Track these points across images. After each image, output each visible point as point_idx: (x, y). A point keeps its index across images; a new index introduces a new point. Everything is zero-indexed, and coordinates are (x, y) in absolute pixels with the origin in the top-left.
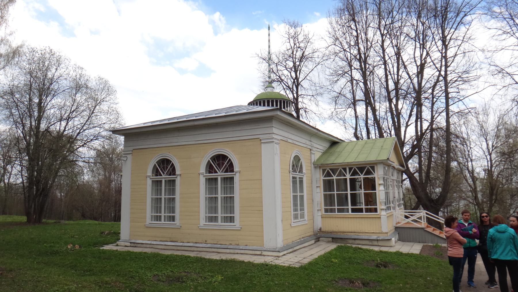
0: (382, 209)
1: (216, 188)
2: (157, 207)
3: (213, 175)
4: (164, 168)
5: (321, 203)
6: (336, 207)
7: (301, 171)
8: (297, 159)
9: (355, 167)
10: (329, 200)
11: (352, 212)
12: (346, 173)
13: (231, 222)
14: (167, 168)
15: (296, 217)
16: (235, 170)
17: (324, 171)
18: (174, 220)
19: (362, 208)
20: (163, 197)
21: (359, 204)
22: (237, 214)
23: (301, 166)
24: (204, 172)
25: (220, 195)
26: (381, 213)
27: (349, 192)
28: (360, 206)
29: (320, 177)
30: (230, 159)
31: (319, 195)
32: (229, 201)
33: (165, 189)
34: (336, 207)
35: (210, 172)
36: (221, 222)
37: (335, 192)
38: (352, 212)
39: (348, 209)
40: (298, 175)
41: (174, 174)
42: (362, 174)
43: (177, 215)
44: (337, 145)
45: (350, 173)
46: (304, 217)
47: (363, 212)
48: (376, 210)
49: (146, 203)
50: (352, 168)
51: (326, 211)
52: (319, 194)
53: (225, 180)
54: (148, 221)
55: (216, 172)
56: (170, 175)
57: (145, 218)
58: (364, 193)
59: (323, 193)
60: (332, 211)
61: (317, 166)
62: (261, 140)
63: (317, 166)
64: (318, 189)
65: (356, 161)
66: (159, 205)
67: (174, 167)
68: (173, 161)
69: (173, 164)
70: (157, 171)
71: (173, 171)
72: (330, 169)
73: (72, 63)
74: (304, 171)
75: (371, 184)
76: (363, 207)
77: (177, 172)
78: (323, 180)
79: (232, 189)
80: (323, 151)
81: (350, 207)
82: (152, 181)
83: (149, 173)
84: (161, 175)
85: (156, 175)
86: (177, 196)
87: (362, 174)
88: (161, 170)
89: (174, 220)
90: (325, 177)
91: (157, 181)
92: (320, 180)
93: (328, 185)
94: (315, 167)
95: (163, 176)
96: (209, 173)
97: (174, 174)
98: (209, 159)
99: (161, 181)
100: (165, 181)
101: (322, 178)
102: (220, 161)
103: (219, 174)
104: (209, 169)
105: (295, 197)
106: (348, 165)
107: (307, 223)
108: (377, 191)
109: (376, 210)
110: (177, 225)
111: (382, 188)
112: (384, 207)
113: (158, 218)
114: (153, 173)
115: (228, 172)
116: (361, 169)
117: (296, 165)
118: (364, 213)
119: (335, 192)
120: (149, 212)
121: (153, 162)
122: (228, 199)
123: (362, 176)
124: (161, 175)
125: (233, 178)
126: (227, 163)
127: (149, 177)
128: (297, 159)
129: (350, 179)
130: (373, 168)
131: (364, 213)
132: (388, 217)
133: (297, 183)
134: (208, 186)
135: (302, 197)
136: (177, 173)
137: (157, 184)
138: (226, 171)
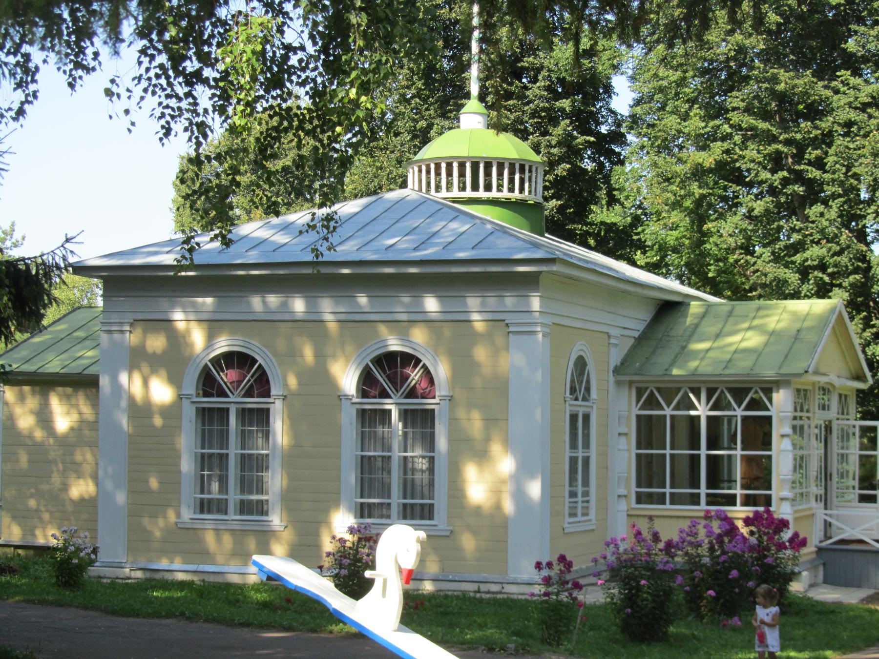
0: (782, 499)
3: (215, 401)
5: (628, 479)
8: (581, 364)
9: (722, 387)
11: (639, 501)
13: (430, 519)
16: (272, 394)
17: (640, 393)
19: (664, 494)
21: (726, 485)
23: (588, 382)
27: (703, 452)
28: (729, 488)
35: (206, 394)
36: (235, 514)
38: (709, 503)
39: (699, 495)
42: (739, 407)
46: (587, 514)
47: (664, 503)
50: (716, 389)
51: (640, 499)
53: (246, 415)
58: (743, 456)
59: (634, 451)
64: (623, 438)
65: (727, 372)
68: (260, 361)
72: (659, 390)
74: (594, 394)
75: (759, 432)
76: (738, 491)
78: (638, 417)
81: (703, 491)
82: (197, 408)
89: (431, 518)
90: (711, 409)
92: (628, 417)
93: (648, 431)
97: (267, 394)
98: (367, 361)
100: (237, 409)
101: (636, 411)
104: (204, 385)
105: (573, 461)
106: (704, 382)
107: (593, 527)
108: (774, 453)
110: (440, 527)
111: (786, 444)
112: (787, 493)
115: (252, 397)
116: (739, 393)
118: (668, 506)
119: (668, 452)
122: (216, 461)
123: (740, 412)
124: (227, 396)
125: (268, 410)
126: (252, 377)
127: (188, 397)
128: (581, 364)
131: (668, 506)
135: (586, 461)
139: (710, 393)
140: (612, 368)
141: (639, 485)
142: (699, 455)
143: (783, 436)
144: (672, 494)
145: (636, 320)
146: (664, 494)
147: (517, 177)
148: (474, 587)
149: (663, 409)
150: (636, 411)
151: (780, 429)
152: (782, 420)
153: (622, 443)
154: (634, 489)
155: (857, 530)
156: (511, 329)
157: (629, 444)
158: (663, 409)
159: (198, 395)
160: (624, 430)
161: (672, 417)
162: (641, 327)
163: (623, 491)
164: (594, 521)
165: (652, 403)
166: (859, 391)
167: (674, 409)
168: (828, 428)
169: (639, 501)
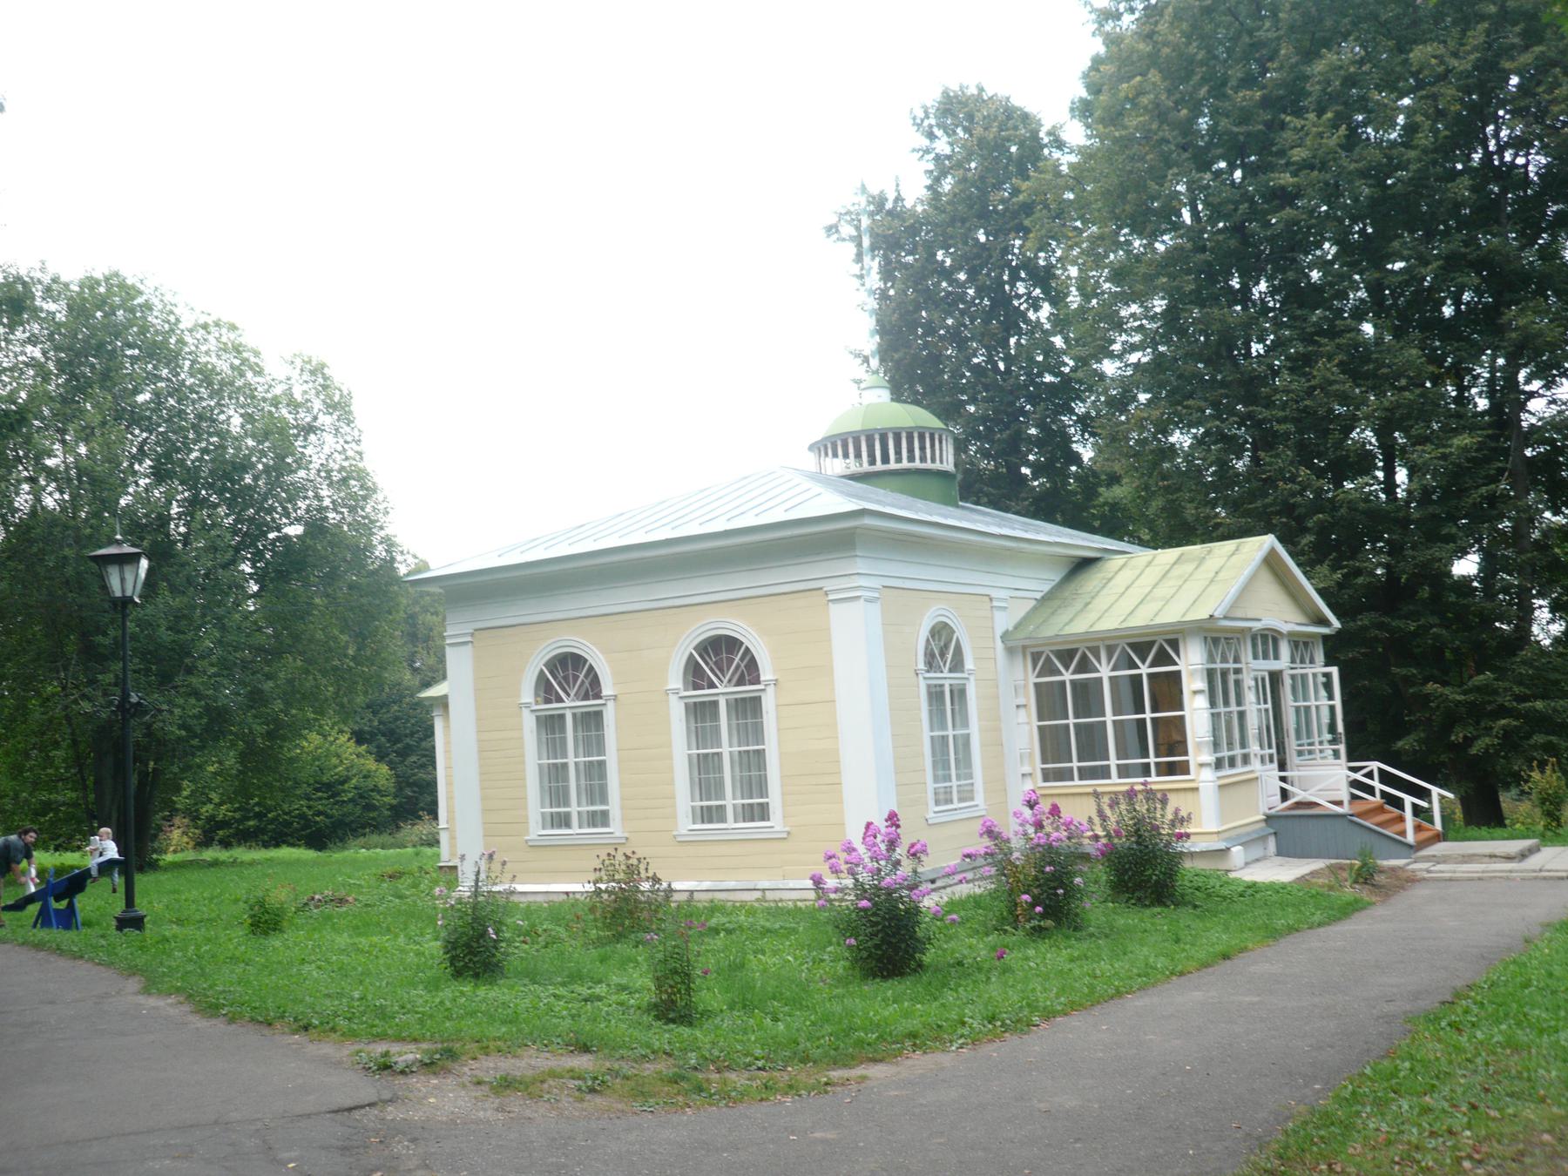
0: (1202, 765)
1: (716, 730)
2: (1239, 703)
4: (566, 678)
5: (1031, 755)
6: (1075, 764)
7: (958, 665)
8: (941, 632)
9: (1160, 640)
10: (1052, 745)
11: (1046, 779)
12: (1099, 662)
13: (763, 819)
14: (576, 678)
15: (943, 798)
17: (1036, 657)
18: (605, 823)
19: (1071, 769)
20: (571, 760)
22: (774, 799)
23: (958, 649)
24: (680, 685)
25: (727, 749)
26: (1198, 774)
29: (1022, 680)
30: (747, 649)
31: (1023, 730)
32: (753, 762)
33: (576, 738)
34: (1075, 764)
35: (696, 687)
37: (1071, 721)
40: (946, 678)
41: (598, 696)
43: (614, 806)
44: (1100, 564)
45: (1109, 660)
48: (1183, 768)
49: (524, 779)
51: (1047, 776)
52: (1027, 728)
54: (536, 831)
55: (712, 685)
56: (586, 698)
57: (525, 822)
59: (1036, 723)
60: (1065, 775)
61: (1018, 646)
62: (826, 594)
63: (1018, 646)
64: (1022, 711)
66: (1234, 708)
67: (596, 676)
68: (590, 661)
69: (591, 668)
70: (548, 688)
71: (593, 687)
73: (388, 531)
74: (969, 664)
75: (1168, 690)
77: (607, 690)
79: (758, 733)
80: (1038, 596)
81: (1113, 762)
82: (538, 718)
83: (527, 695)
84: (561, 701)
85: (548, 701)
86: (611, 757)
87: (1143, 662)
88: (560, 684)
89: (605, 823)
91: (552, 716)
92: (1025, 686)
93: (1049, 701)
94: (1010, 651)
95: (568, 703)
96: (695, 689)
97: (598, 696)
99: (562, 717)
100: (574, 715)
101: (1033, 679)
102: (721, 654)
103: (721, 689)
105: (940, 745)
106: (1102, 639)
108: (1187, 713)
109: (1183, 768)
110: (617, 834)
111: (1202, 702)
113: (563, 821)
114: (537, 695)
117: (942, 648)
119: (1071, 721)
120: (535, 807)
121: (536, 663)
124: (561, 701)
126: (742, 659)
127: (527, 705)
128: (941, 632)
129: (1111, 678)
130: (1174, 644)
131: (1077, 782)
132: (1221, 787)
133: (946, 703)
134: (693, 725)
136: (604, 693)
137: (551, 725)
138: (740, 682)
139: (1110, 650)
140: (999, 633)
141: (1044, 761)
142: (1104, 723)
143: (1195, 692)
144: (1080, 769)
145: (1039, 583)
146: (1071, 769)
147: (928, 451)
148: (758, 895)
149: (1060, 674)
150: (1033, 679)
151: (1193, 684)
152: (1192, 674)
153: (1022, 715)
154: (1039, 765)
155: (1312, 791)
156: (831, 597)
157: (1029, 716)
158: (1060, 674)
159: (537, 703)
160: (1021, 701)
161: (1072, 682)
162: (1047, 588)
163: (1027, 769)
164: (982, 806)
165: (1049, 669)
166: (1325, 638)
167: (1075, 672)
168: (1275, 677)
169: (1046, 779)
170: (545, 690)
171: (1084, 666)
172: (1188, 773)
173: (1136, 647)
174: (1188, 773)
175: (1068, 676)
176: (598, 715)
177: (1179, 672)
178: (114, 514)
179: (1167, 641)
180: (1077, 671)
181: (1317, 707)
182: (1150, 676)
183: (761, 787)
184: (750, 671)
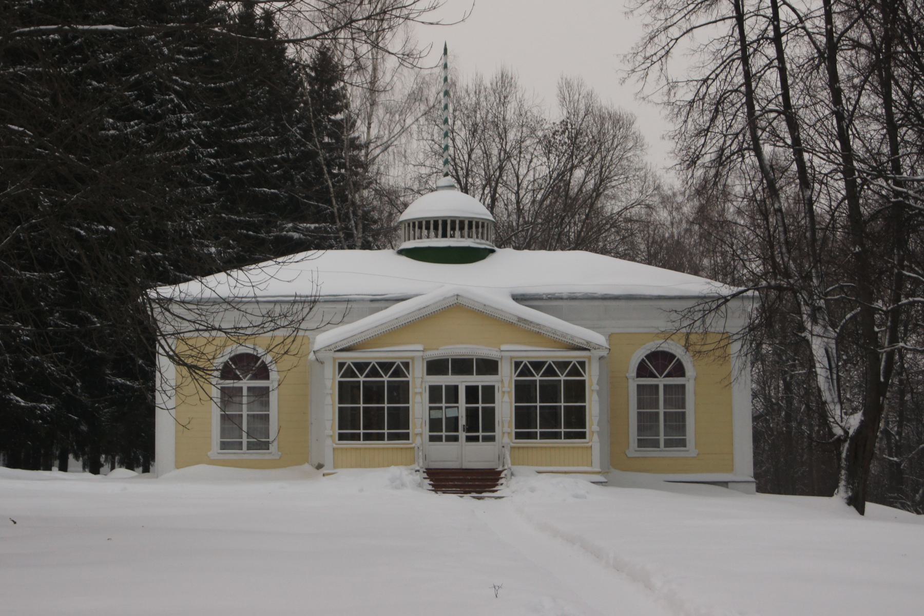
6: (362, 431)
11: (516, 438)
19: (441, 436)
34: (563, 430)
37: (538, 404)
75: (401, 392)
81: (245, 440)
101: (514, 378)
119: (538, 404)
150: (338, 379)
157: (510, 399)
167: (390, 377)
169: (516, 438)
170: (642, 371)
171: (374, 373)
172: (408, 439)
173: (382, 365)
174: (408, 439)
175: (562, 378)
176: (265, 391)
177: (584, 381)
178: (156, 42)
179: (579, 362)
180: (392, 376)
181: (440, 408)
182: (565, 381)
183: (682, 429)
184: (679, 371)
